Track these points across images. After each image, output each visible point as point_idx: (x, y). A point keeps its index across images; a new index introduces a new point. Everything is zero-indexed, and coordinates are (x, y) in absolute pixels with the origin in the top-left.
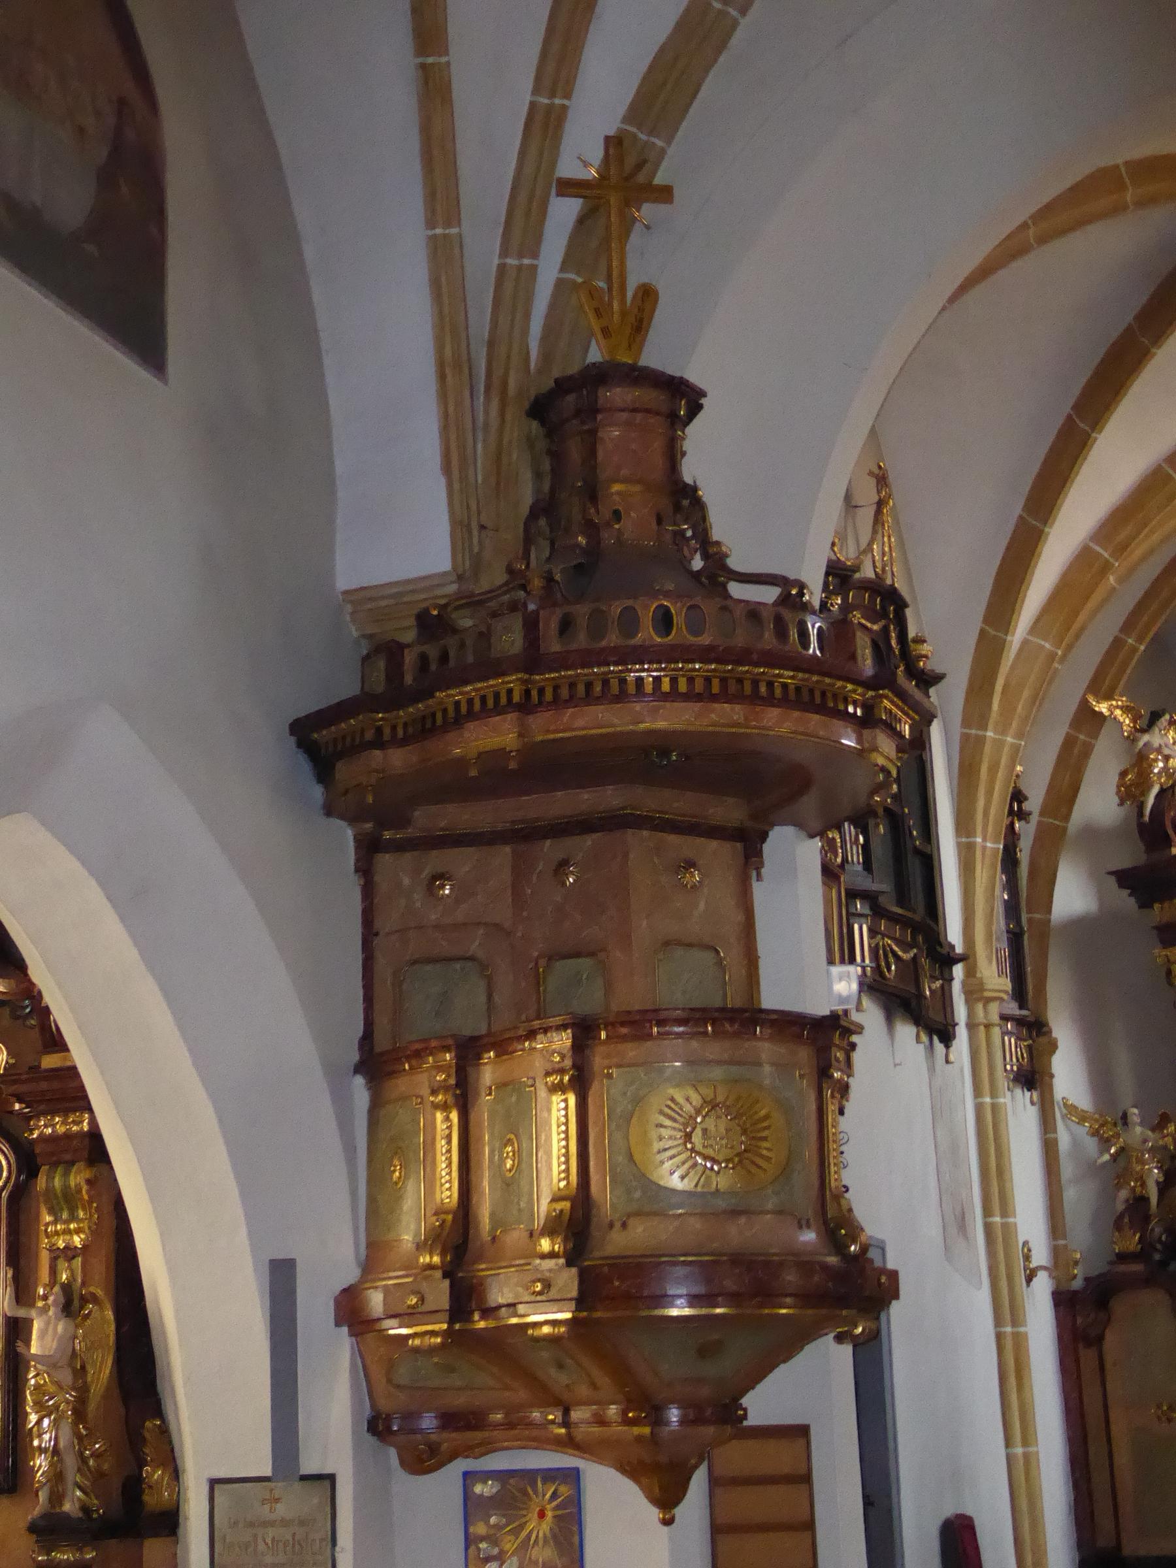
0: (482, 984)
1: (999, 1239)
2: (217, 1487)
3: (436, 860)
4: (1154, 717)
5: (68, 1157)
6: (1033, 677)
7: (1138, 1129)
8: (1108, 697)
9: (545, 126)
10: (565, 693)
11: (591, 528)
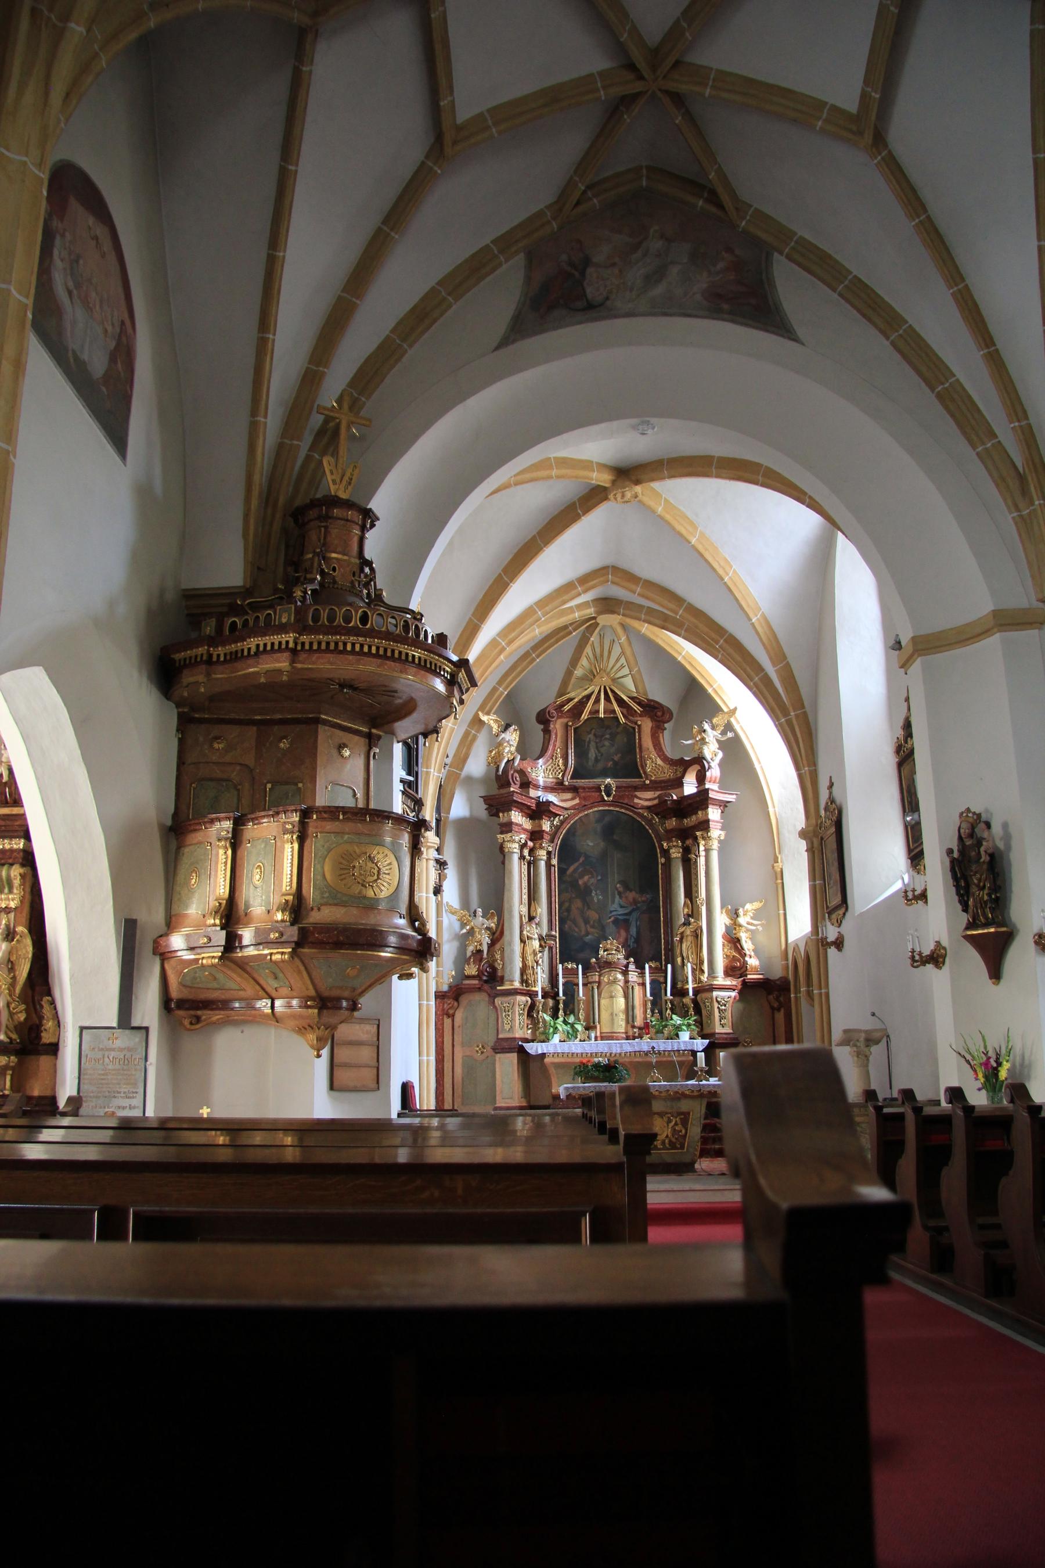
0: (236, 793)
2: (85, 1031)
3: (216, 730)
4: (507, 727)
5: (10, 861)
8: (488, 714)
10: (323, 646)
11: (322, 573)
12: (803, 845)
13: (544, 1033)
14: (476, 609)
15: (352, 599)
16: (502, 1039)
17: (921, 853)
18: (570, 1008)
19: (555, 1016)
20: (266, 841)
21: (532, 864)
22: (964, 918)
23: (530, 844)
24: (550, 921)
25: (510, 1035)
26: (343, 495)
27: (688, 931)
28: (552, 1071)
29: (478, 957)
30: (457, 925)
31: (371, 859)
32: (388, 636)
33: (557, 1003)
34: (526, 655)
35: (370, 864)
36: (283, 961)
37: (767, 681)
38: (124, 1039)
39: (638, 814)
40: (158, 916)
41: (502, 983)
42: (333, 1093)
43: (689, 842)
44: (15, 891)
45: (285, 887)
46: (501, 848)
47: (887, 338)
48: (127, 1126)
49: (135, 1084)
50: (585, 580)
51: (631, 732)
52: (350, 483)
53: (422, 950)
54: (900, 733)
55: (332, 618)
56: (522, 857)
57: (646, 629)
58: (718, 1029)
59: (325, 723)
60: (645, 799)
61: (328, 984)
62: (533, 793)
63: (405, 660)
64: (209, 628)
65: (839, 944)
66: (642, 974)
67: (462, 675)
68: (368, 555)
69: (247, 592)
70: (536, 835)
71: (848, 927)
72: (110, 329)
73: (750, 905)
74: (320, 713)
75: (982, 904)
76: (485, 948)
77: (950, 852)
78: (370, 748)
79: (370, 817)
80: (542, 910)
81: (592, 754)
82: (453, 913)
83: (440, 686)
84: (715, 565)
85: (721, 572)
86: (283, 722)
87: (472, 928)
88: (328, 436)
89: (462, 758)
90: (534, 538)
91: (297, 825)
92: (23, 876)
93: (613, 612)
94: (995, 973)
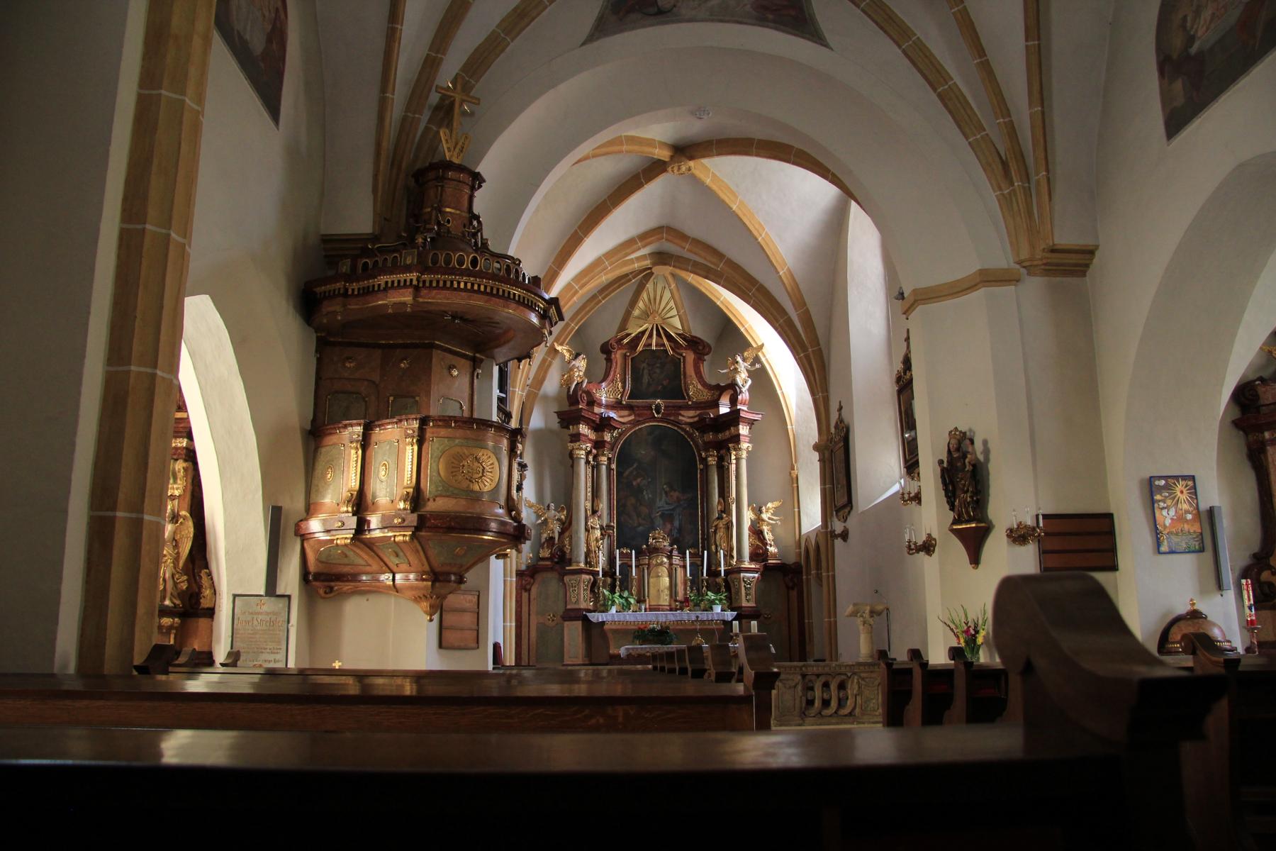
4: (577, 355)
8: (561, 344)
9: (431, 64)
10: (441, 284)
11: (439, 224)
12: (816, 456)
13: (604, 605)
14: (556, 259)
15: (462, 246)
17: (917, 463)
18: (625, 585)
19: (613, 591)
20: (391, 443)
21: (596, 468)
22: (951, 516)
23: (594, 451)
24: (610, 514)
26: (456, 161)
27: (721, 524)
28: (610, 635)
30: (533, 517)
31: (477, 459)
32: (494, 277)
33: (614, 580)
34: (594, 297)
36: (405, 542)
37: (790, 323)
38: (270, 605)
39: (684, 430)
40: (300, 504)
43: (723, 452)
45: (406, 481)
46: (571, 455)
47: (899, 46)
48: (271, 673)
49: (279, 642)
50: (645, 237)
51: (677, 364)
53: (517, 535)
54: (900, 366)
55: (448, 261)
56: (587, 462)
57: (692, 279)
58: (744, 604)
60: (688, 416)
61: (439, 560)
62: (597, 410)
63: (507, 298)
64: (345, 267)
65: (844, 536)
66: (684, 558)
67: (553, 311)
68: (476, 210)
69: (374, 238)
70: (599, 444)
71: (852, 523)
72: (267, 14)
73: (772, 502)
75: (966, 505)
77: (941, 462)
79: (474, 425)
80: (603, 506)
81: (646, 379)
83: (534, 319)
84: (751, 228)
85: (755, 233)
86: (405, 346)
88: (445, 112)
89: (539, 381)
92: (185, 469)
93: (665, 264)
94: (975, 559)
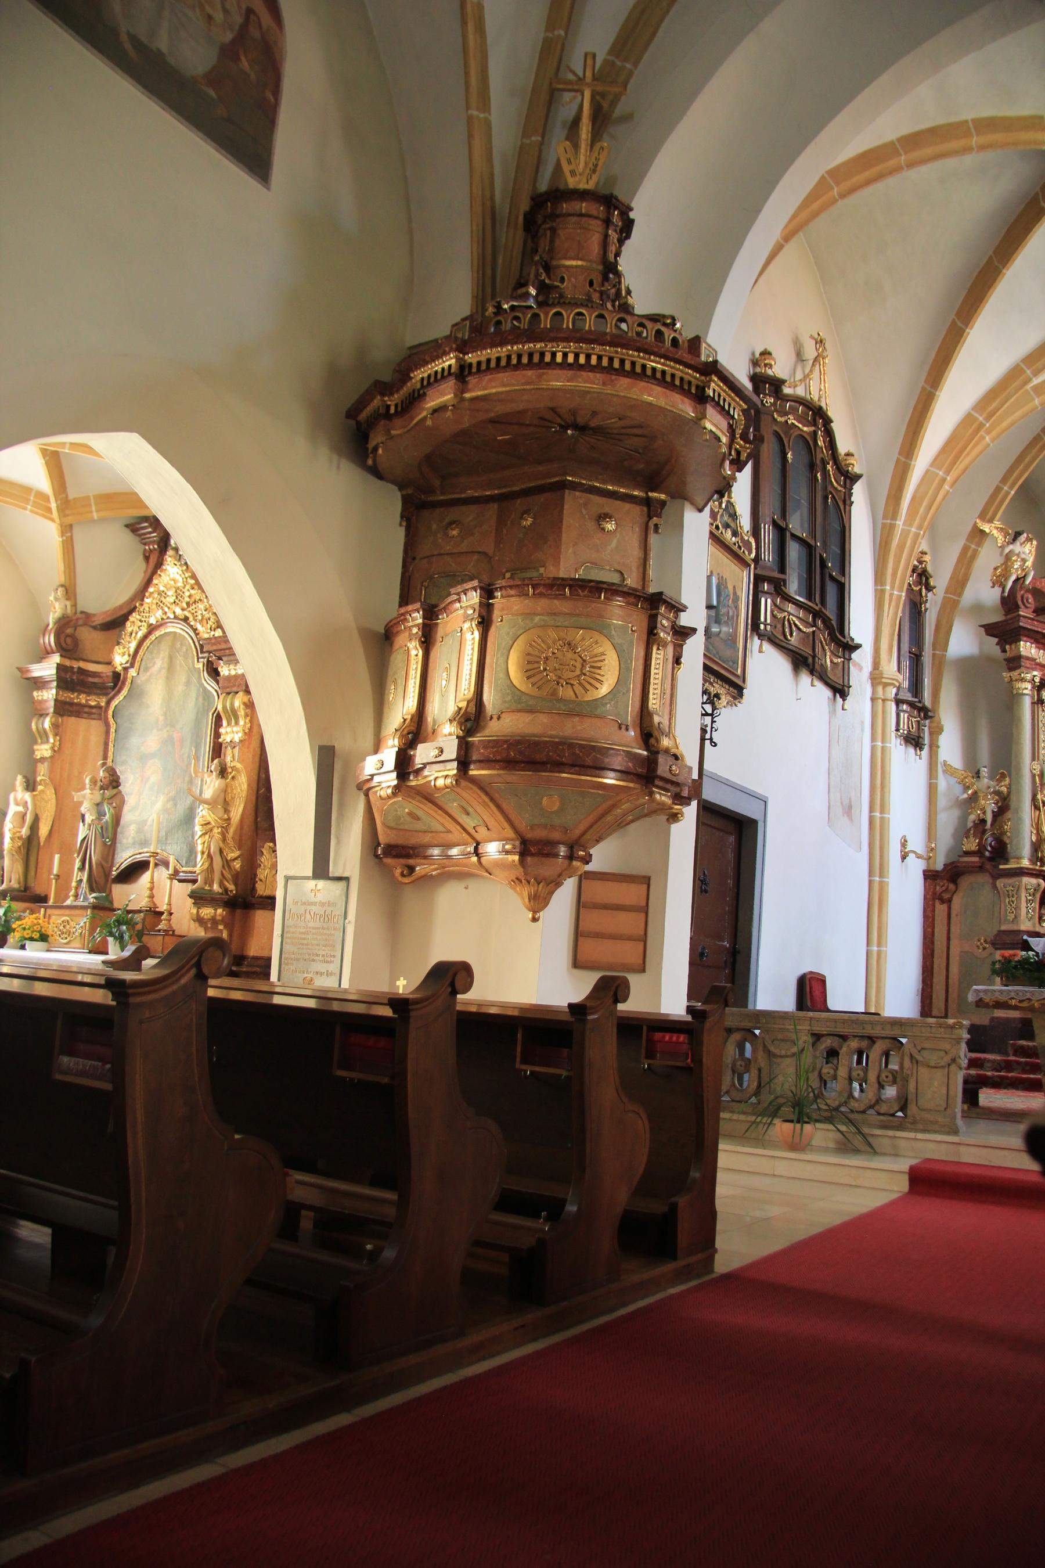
1: (878, 829)
3: (454, 513)
4: (1017, 535)
5: (235, 689)
6: (931, 492)
7: (986, 780)
14: (929, 374)
16: (1004, 932)
25: (1015, 928)
29: (981, 827)
30: (958, 789)
35: (570, 655)
41: (1007, 861)
42: (576, 971)
44: (242, 722)
52: (594, 171)
59: (574, 486)
72: (219, 16)
74: (566, 474)
76: (989, 818)
78: (650, 517)
82: (952, 775)
87: (975, 793)
90: (990, 261)
91: (477, 607)
